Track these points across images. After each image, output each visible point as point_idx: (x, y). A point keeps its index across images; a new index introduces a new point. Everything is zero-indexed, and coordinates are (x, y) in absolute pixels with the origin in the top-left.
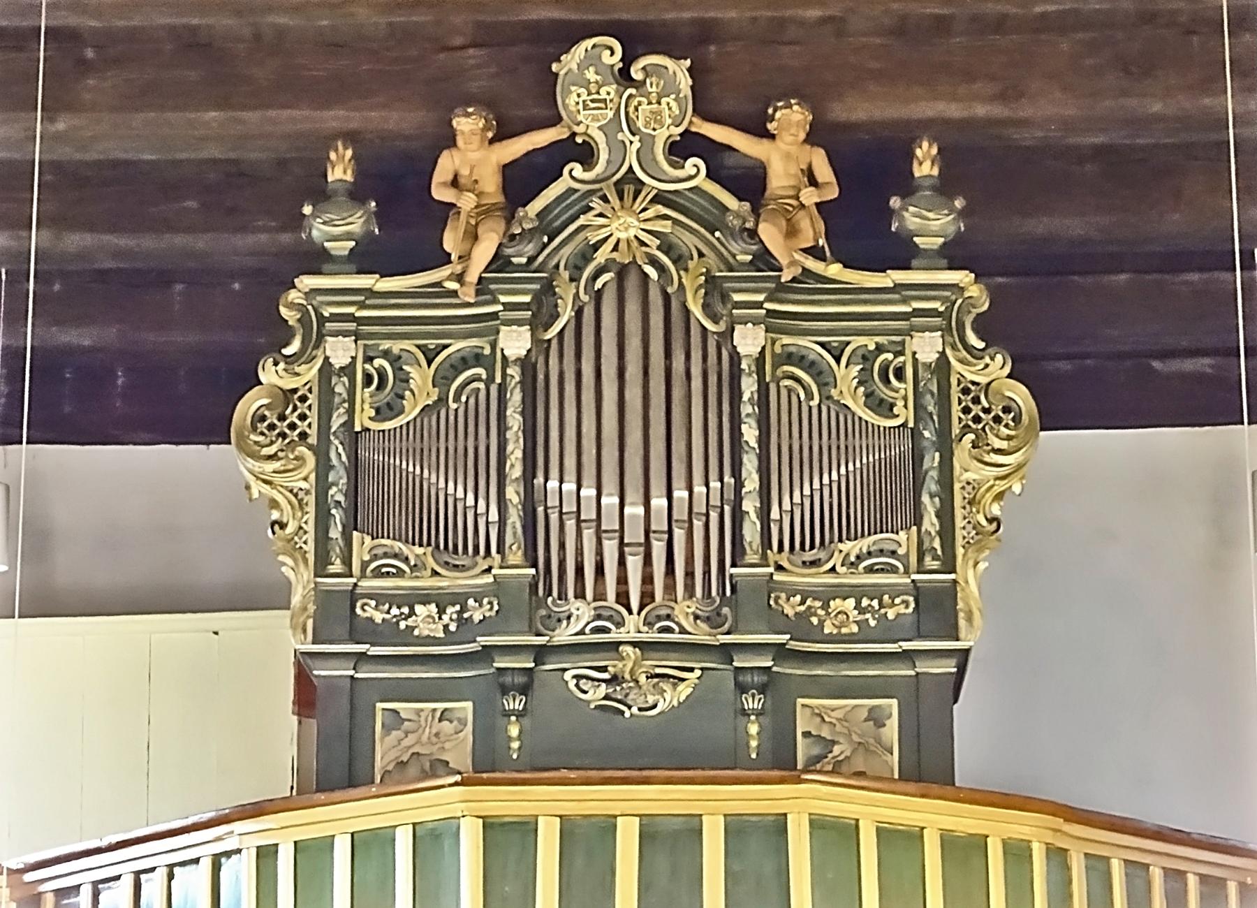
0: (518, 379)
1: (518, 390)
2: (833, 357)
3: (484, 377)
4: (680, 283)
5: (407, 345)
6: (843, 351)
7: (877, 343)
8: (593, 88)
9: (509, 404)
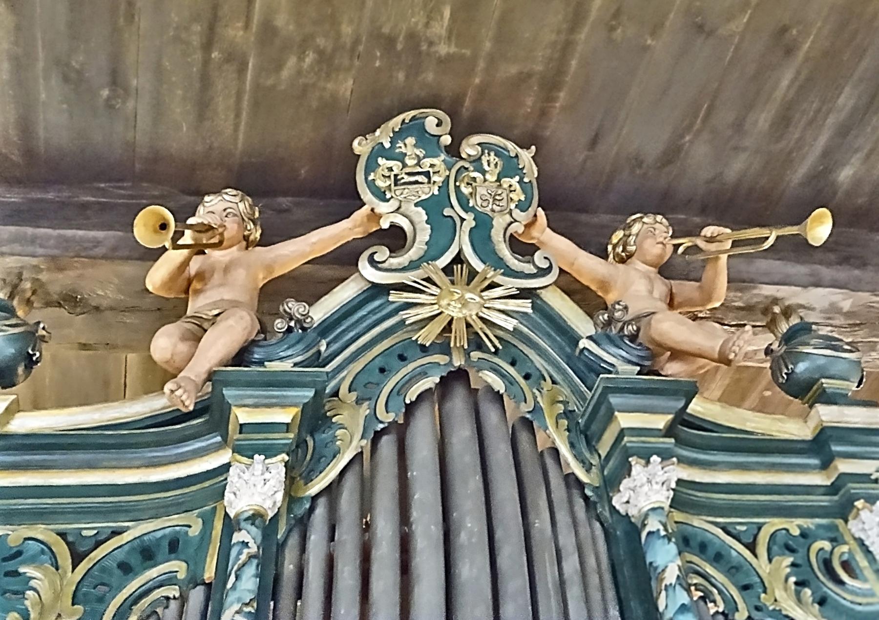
0: (253, 549)
1: (251, 570)
2: (747, 546)
3: (181, 576)
4: (536, 403)
5: (40, 531)
6: (755, 537)
7: (799, 527)
8: (410, 162)
9: (231, 597)
